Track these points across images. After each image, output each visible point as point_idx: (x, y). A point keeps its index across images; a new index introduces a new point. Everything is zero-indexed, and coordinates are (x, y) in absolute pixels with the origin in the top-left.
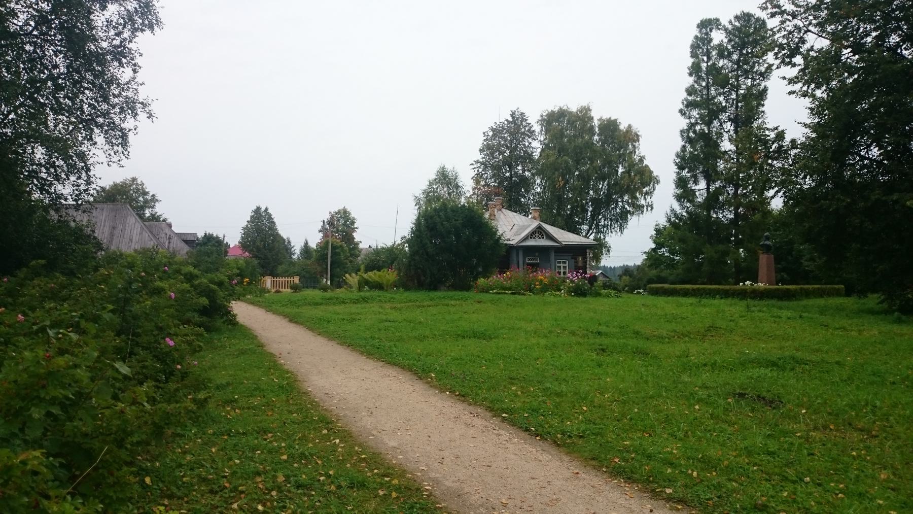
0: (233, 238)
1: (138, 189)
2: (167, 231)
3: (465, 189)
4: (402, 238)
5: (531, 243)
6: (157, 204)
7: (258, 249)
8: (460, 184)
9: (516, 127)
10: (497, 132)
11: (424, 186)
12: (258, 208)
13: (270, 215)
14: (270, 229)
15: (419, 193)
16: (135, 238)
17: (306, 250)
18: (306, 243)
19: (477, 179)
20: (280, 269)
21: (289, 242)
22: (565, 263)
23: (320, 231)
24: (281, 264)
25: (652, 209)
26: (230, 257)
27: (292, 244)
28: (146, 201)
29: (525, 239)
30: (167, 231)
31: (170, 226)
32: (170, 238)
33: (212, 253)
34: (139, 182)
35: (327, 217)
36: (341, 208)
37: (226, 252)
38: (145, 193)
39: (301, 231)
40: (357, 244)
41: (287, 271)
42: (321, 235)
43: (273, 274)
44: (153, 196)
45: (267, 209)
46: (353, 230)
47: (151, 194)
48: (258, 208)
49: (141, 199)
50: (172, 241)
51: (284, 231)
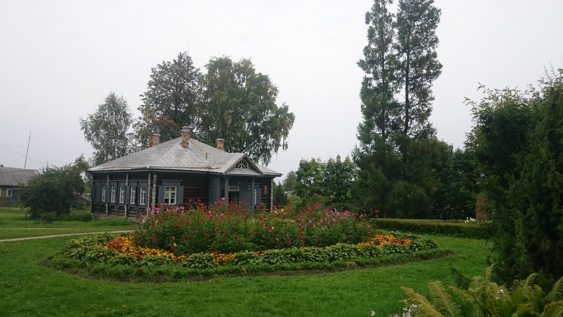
3: (133, 117)
5: (237, 172)
8: (128, 113)
10: (164, 68)
11: (94, 110)
19: (146, 110)
22: (173, 189)
29: (232, 168)
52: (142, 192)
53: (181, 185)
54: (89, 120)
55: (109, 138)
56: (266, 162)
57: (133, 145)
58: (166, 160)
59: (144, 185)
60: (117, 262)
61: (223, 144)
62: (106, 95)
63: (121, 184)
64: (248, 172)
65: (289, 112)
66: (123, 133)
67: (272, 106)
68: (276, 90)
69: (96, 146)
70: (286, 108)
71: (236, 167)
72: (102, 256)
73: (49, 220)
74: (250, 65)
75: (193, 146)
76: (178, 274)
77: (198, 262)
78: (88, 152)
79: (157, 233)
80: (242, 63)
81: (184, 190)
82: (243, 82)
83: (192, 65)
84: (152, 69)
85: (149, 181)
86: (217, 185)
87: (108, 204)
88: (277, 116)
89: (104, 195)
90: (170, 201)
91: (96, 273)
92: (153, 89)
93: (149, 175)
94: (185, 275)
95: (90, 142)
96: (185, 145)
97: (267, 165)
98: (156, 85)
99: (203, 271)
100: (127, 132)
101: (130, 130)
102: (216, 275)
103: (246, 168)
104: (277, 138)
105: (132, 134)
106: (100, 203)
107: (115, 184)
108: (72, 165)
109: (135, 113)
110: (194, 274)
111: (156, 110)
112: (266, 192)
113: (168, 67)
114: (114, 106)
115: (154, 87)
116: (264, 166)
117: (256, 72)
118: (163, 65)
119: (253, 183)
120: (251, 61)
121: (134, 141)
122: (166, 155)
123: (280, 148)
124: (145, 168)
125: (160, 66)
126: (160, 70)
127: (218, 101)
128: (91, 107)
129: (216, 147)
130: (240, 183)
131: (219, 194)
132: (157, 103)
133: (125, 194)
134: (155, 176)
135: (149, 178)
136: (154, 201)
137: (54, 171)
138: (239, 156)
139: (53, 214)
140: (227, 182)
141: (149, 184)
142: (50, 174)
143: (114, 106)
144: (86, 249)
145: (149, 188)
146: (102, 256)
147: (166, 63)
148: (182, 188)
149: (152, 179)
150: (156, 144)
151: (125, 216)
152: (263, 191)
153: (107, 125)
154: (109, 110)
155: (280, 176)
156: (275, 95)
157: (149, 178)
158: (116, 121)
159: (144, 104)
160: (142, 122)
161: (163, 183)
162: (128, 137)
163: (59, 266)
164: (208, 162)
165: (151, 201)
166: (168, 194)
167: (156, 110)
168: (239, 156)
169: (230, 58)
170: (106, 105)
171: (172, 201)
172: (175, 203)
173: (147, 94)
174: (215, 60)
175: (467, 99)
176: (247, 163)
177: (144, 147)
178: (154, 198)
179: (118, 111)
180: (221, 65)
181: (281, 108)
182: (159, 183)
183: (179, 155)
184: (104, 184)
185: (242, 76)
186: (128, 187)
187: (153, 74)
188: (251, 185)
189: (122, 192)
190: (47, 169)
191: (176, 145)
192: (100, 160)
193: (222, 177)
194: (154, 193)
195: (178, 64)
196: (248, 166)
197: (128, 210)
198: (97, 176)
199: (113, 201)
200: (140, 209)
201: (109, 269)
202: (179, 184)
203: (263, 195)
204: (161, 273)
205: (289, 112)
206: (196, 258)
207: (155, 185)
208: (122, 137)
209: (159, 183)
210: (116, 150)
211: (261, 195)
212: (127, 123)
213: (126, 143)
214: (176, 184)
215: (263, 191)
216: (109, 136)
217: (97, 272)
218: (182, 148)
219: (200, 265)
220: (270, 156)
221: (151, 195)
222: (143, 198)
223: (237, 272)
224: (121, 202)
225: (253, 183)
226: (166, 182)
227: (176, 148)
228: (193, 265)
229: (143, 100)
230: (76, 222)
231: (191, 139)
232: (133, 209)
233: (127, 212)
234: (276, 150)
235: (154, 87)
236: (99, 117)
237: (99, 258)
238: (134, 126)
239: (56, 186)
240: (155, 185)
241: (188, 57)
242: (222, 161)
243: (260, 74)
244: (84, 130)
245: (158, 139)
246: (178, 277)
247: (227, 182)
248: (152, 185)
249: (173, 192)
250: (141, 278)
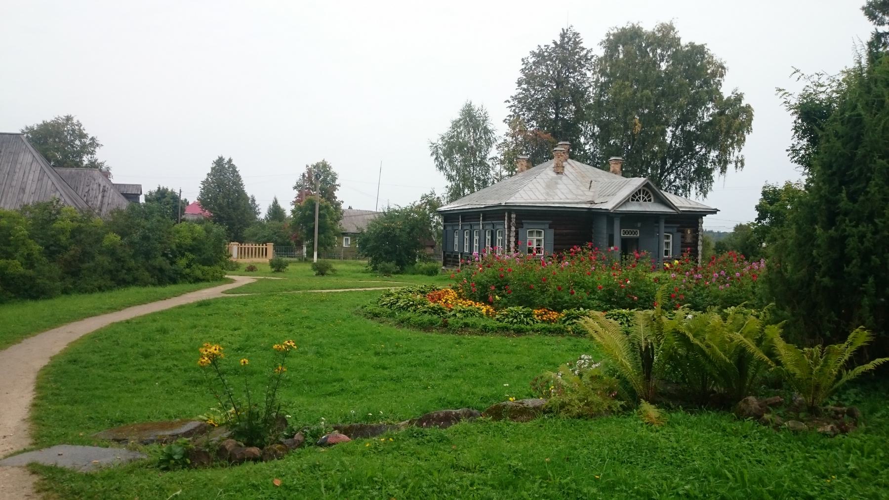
0: (190, 192)
1: (73, 131)
2: (101, 180)
3: (496, 134)
4: (423, 198)
5: (634, 207)
6: (97, 149)
7: (221, 207)
8: (490, 128)
9: (567, 52)
10: (541, 57)
11: (445, 128)
12: (221, 159)
13: (234, 167)
14: (234, 183)
15: (437, 140)
16: (30, 187)
17: (276, 212)
18: (276, 202)
19: (514, 122)
20: (247, 232)
21: (253, 200)
22: (539, 233)
23: (295, 188)
24: (248, 225)
25: (742, 165)
26: (189, 215)
27: (257, 203)
28: (84, 146)
29: (626, 202)
30: (101, 180)
31: (106, 174)
32: (104, 191)
33: (151, 213)
34: (75, 121)
35: (304, 170)
36: (320, 160)
37: (183, 210)
38: (82, 136)
39: (271, 189)
40: (338, 204)
41: (256, 235)
42: (296, 192)
43: (241, 241)
44: (93, 139)
45: (230, 160)
46: (334, 188)
47: (90, 137)
48: (221, 159)
49: (77, 142)
50: (107, 194)
51: (249, 190)
52: (499, 238)
54: (440, 142)
55: (466, 166)
56: (704, 191)
57: (497, 174)
58: (530, 193)
60: (425, 312)
61: (619, 165)
62: (460, 106)
65: (743, 104)
66: (484, 158)
67: (714, 95)
68: (723, 68)
69: (450, 178)
70: (739, 98)
71: (633, 200)
72: (412, 305)
73: (387, 272)
74: (672, 33)
75: (571, 170)
76: (485, 327)
77: (512, 317)
78: (438, 184)
79: (479, 283)
80: (659, 31)
81: (555, 235)
82: (662, 60)
83: (581, 45)
84: (523, 60)
86: (603, 227)
87: (462, 254)
88: (722, 113)
89: (456, 242)
91: (402, 323)
92: (524, 90)
94: (493, 329)
95: (442, 173)
96: (559, 170)
97: (705, 196)
98: (528, 83)
99: (515, 326)
100: (489, 156)
101: (494, 152)
102: (531, 332)
103: (650, 200)
104: (724, 150)
105: (496, 158)
107: (468, 227)
108: (416, 204)
109: (500, 130)
110: (505, 329)
111: (529, 121)
113: (546, 54)
114: (471, 120)
115: (525, 86)
116: (701, 196)
117: (683, 43)
118: (537, 52)
119: (662, 225)
120: (674, 25)
121: (498, 167)
122: (530, 185)
123: (731, 167)
124: (500, 205)
125: (533, 54)
126: (534, 59)
127: (618, 97)
128: (441, 124)
129: (608, 170)
130: (639, 225)
131: (604, 241)
132: (529, 110)
134: (513, 216)
137: (397, 211)
138: (637, 182)
139: (391, 265)
140: (617, 224)
142: (390, 216)
143: (471, 120)
144: (399, 298)
146: (412, 305)
147: (543, 47)
148: (552, 231)
150: (522, 171)
153: (462, 149)
154: (466, 127)
155: (715, 213)
156: (722, 76)
158: (475, 141)
159: (512, 113)
160: (509, 139)
161: (525, 226)
162: (490, 163)
163: (369, 315)
164: (592, 194)
167: (529, 121)
168: (637, 182)
169: (641, 25)
170: (460, 120)
173: (514, 98)
174: (615, 31)
175: (780, 90)
177: (511, 176)
179: (476, 127)
180: (627, 38)
181: (729, 99)
182: (519, 225)
183: (551, 186)
184: (456, 228)
185: (659, 51)
187: (523, 67)
188: (658, 227)
189: (476, 238)
190: (389, 208)
191: (547, 170)
192: (456, 194)
193: (609, 216)
194: (513, 239)
195: (561, 46)
196: (652, 198)
198: (449, 217)
201: (415, 318)
202: (547, 226)
203: (684, 245)
204: (466, 325)
205: (743, 104)
206: (512, 312)
207: (513, 229)
208: (482, 163)
209: (519, 225)
210: (475, 182)
212: (489, 143)
213: (487, 171)
215: (683, 237)
216: (466, 164)
217: (403, 322)
218: (554, 175)
219: (515, 321)
220: (710, 180)
221: (509, 242)
223: (560, 332)
225: (662, 225)
226: (528, 223)
227: (546, 174)
228: (506, 320)
229: (510, 107)
230: (420, 276)
231: (570, 161)
234: (723, 170)
235: (525, 86)
236: (452, 138)
237: (408, 307)
238: (498, 147)
239: (398, 231)
240: (513, 229)
241: (575, 33)
242: (609, 190)
243: (692, 45)
244: (435, 156)
246: (485, 330)
247: (617, 224)
248: (509, 227)
250: (444, 329)
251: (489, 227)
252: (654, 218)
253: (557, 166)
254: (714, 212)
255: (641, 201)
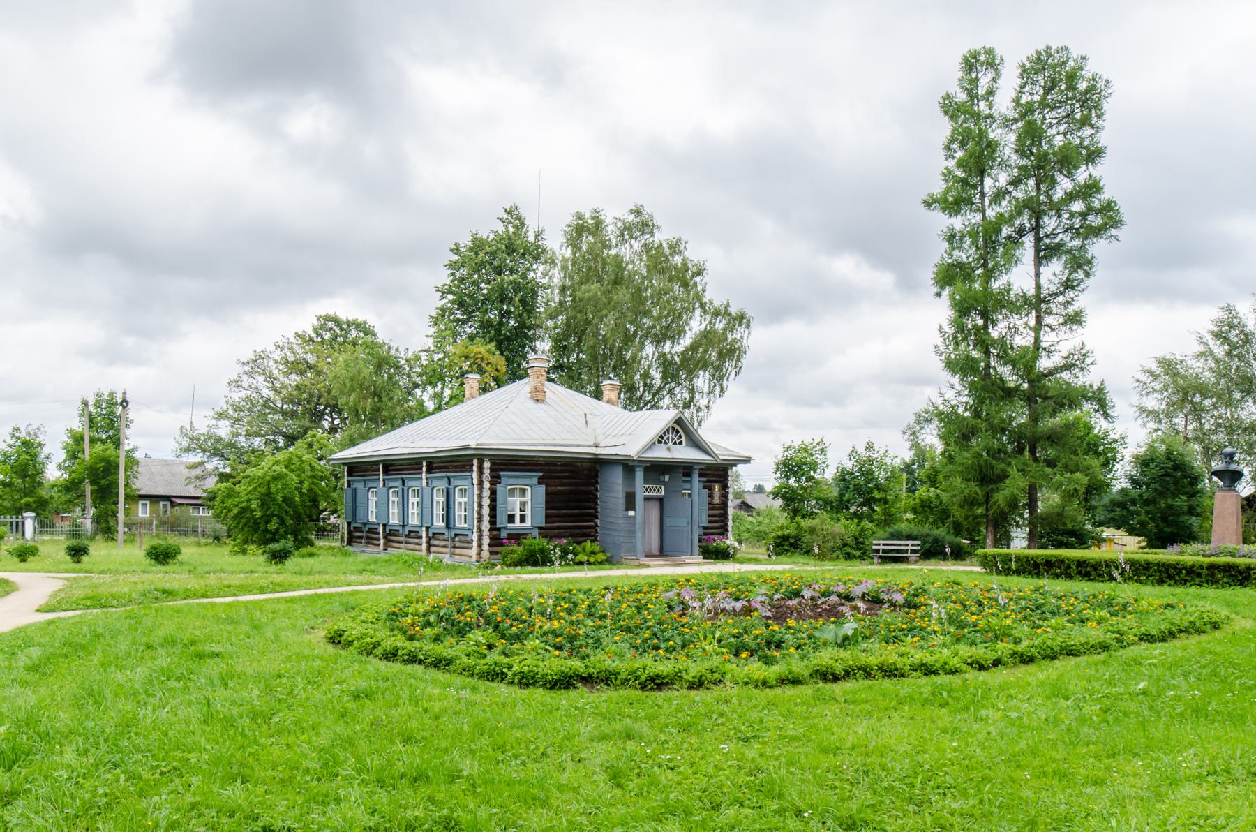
29: (651, 446)
53: (540, 483)
59: (463, 484)
61: (616, 392)
63: (411, 483)
64: (684, 453)
71: (660, 442)
81: (547, 494)
85: (475, 475)
86: (613, 487)
87: (384, 526)
90: (517, 519)
93: (475, 462)
103: (681, 443)
106: (365, 524)
107: (399, 484)
112: (717, 500)
119: (696, 478)
130: (667, 478)
131: (621, 502)
133: (421, 505)
134: (487, 465)
135: (475, 468)
136: (486, 518)
140: (639, 475)
141: (475, 481)
145: (476, 491)
148: (542, 488)
149: (481, 469)
151: (424, 552)
152: (710, 496)
157: (475, 468)
161: (503, 479)
165: (480, 520)
166: (514, 504)
171: (523, 519)
172: (528, 523)
176: (681, 432)
178: (486, 511)
184: (371, 484)
186: (427, 491)
188: (690, 482)
189: (413, 500)
193: (628, 466)
194: (486, 502)
197: (429, 539)
199: (395, 520)
200: (456, 535)
202: (535, 481)
203: (712, 506)
207: (487, 485)
209: (495, 480)
211: (706, 507)
214: (528, 481)
215: (710, 496)
221: (480, 506)
222: (463, 513)
224: (413, 521)
225: (696, 478)
232: (441, 537)
233: (428, 542)
245: (476, 386)
247: (639, 475)
248: (481, 483)
249: (523, 499)
251: (443, 484)
252: (686, 469)
253: (536, 390)
254: (747, 461)
255: (670, 444)
